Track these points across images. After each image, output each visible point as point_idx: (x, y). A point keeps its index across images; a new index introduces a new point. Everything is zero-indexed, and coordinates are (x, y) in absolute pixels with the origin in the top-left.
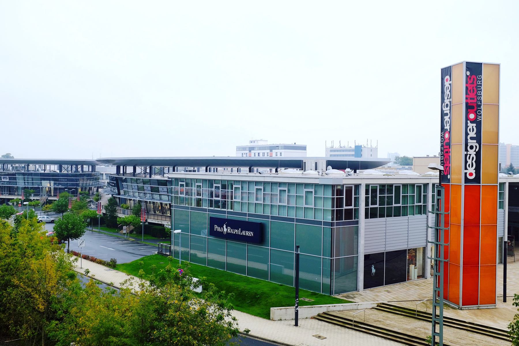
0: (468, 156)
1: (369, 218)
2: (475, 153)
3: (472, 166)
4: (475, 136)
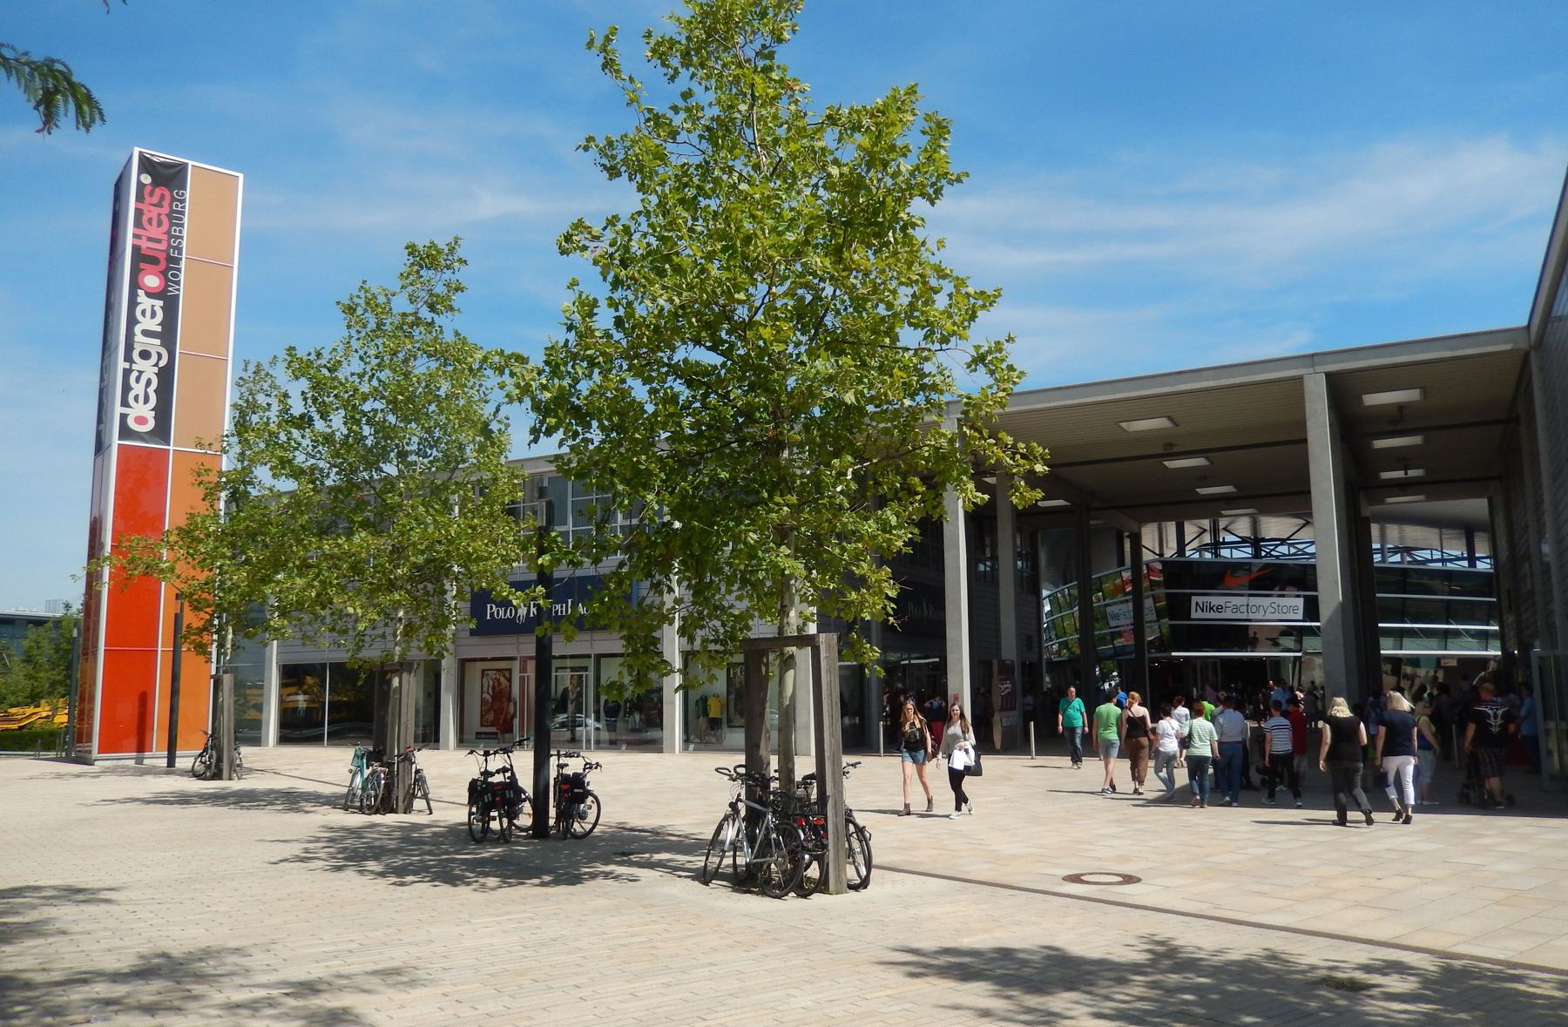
0: (134, 375)
1: (1317, 596)
2: (156, 370)
3: (146, 400)
4: (159, 329)
